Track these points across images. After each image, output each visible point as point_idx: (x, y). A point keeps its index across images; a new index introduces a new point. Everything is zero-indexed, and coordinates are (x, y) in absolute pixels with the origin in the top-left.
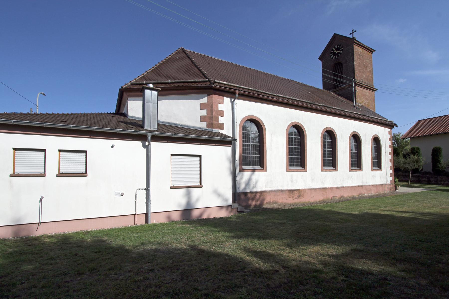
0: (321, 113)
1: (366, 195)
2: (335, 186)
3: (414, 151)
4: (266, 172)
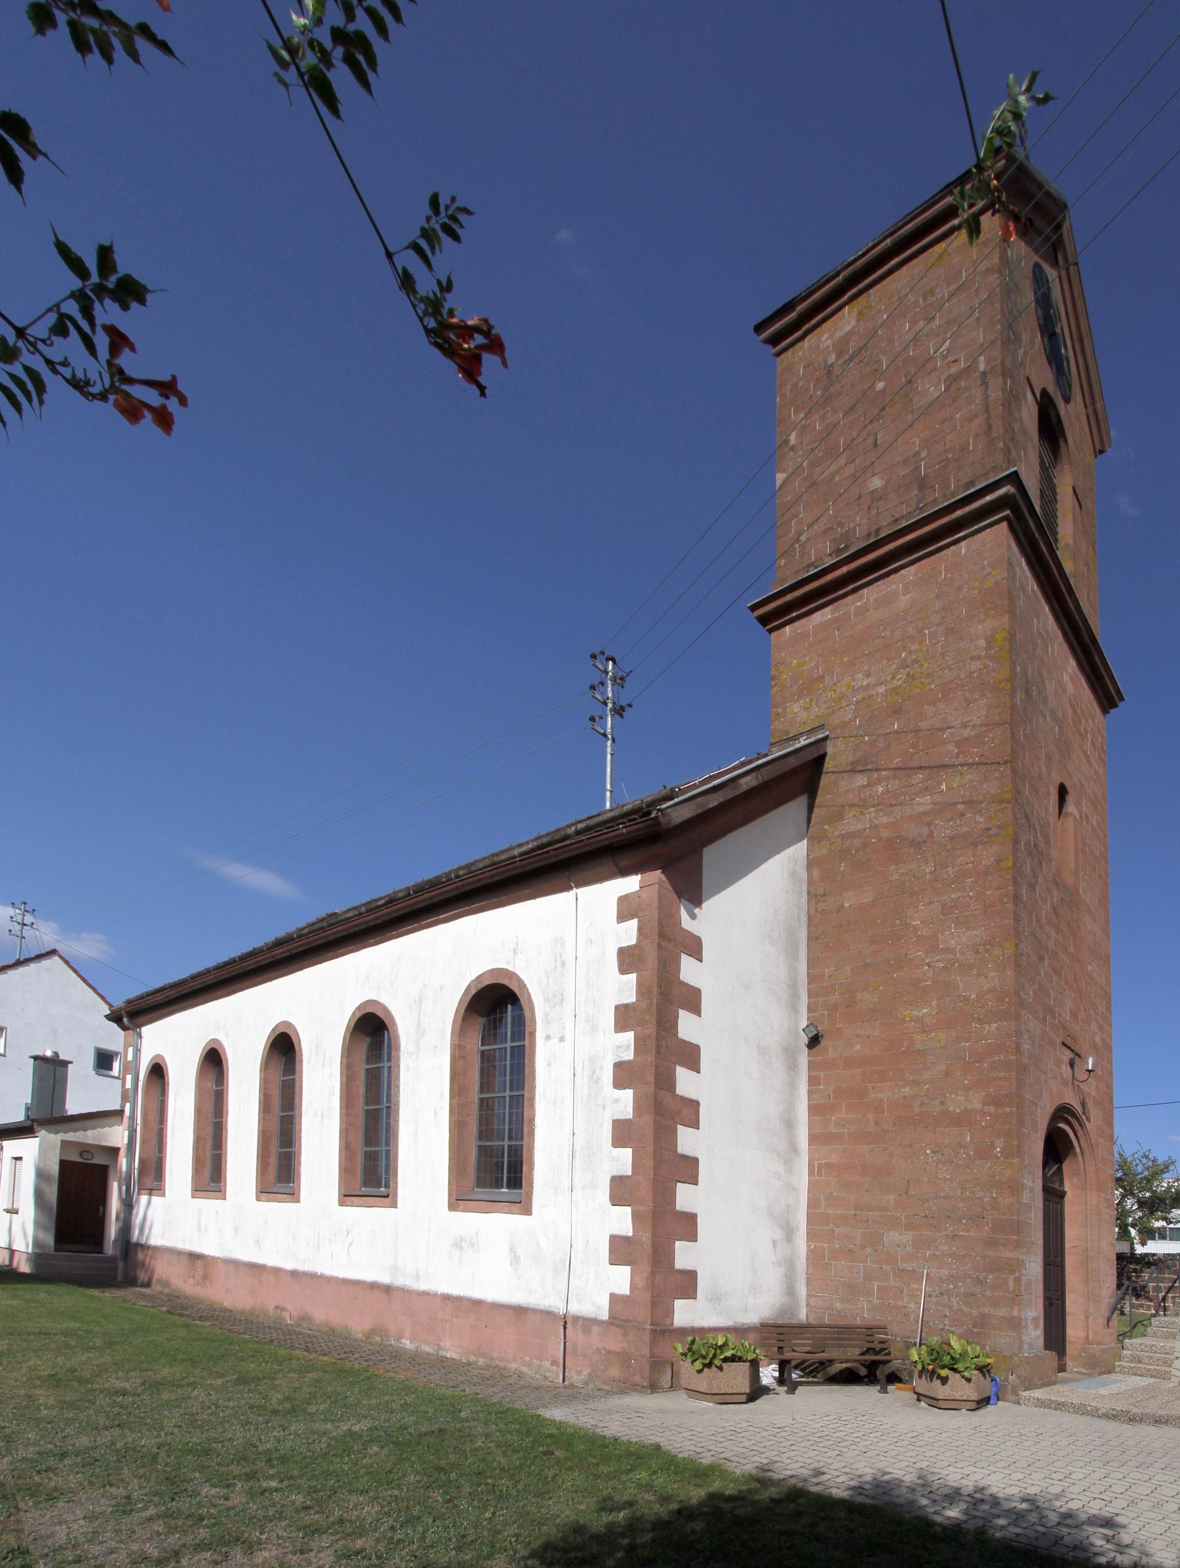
0: (276, 973)
1: (407, 1344)
2: (289, 1266)
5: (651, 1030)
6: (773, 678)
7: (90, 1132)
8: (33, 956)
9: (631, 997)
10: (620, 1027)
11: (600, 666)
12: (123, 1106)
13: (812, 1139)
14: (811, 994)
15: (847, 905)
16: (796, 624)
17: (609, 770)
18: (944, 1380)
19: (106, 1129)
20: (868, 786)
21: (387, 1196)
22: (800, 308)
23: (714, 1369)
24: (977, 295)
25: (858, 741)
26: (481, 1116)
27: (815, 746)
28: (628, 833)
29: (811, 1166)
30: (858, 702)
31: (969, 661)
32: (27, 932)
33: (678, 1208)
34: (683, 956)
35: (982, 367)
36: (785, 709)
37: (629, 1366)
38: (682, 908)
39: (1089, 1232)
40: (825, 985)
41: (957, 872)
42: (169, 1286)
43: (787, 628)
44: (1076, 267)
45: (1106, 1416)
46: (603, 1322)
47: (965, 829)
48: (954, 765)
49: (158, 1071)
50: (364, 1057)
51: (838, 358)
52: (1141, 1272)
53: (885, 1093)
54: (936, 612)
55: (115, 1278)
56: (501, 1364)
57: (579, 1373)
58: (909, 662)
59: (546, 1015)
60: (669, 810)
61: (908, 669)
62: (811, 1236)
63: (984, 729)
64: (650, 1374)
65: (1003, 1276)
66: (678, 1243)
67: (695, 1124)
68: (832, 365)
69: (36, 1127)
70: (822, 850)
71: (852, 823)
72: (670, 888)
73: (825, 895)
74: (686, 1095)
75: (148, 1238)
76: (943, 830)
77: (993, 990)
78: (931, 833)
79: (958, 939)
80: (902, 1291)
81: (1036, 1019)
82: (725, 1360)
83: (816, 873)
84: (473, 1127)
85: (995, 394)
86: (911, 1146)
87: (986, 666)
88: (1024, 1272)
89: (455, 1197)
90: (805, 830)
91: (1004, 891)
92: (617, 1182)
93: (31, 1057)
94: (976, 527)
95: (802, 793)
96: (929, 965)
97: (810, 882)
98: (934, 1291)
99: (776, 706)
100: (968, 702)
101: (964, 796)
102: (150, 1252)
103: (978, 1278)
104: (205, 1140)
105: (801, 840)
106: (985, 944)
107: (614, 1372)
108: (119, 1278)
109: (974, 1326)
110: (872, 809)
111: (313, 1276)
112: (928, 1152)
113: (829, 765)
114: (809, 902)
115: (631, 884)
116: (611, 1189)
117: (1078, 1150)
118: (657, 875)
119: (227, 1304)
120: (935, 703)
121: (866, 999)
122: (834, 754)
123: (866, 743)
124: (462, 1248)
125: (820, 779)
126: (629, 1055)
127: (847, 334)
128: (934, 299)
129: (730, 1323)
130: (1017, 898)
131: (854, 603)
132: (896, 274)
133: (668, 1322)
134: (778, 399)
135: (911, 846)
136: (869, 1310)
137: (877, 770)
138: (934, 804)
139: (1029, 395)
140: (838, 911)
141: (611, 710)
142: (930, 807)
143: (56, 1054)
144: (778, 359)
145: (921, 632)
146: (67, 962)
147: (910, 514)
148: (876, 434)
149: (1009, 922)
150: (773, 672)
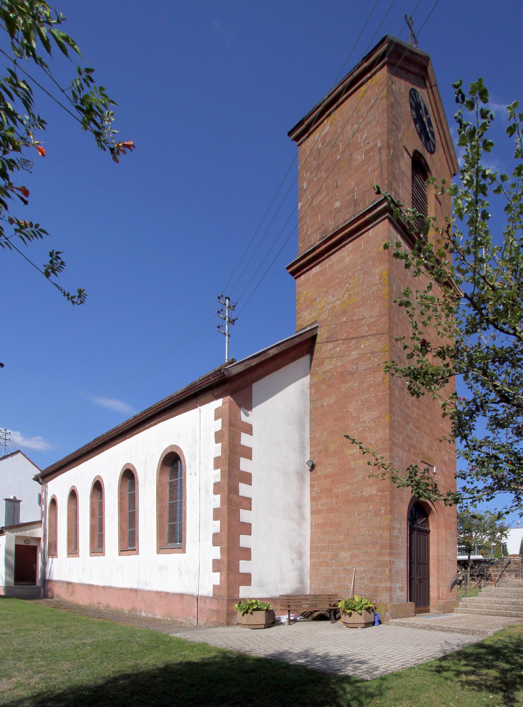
1: (143, 614)
2: (102, 584)
3: (510, 689)
4: (250, 549)
5: (226, 467)
6: (297, 301)
7: (28, 531)
8: (10, 454)
9: (219, 454)
10: (216, 467)
11: (222, 302)
12: (42, 519)
13: (312, 512)
14: (311, 446)
15: (325, 404)
16: (306, 274)
17: (227, 350)
18: (350, 615)
19: (35, 529)
20: (333, 348)
21: (135, 550)
22: (306, 123)
23: (249, 614)
24: (377, 110)
25: (330, 328)
26: (170, 511)
27: (310, 332)
28: (214, 380)
29: (311, 525)
30: (329, 309)
31: (372, 286)
32: (8, 443)
33: (241, 546)
34: (242, 433)
35: (379, 145)
36: (301, 315)
37: (219, 615)
38: (242, 412)
39: (440, 548)
40: (316, 442)
41: (367, 385)
42: (60, 598)
43: (302, 277)
44: (436, 87)
45: (421, 628)
46: (211, 597)
47: (371, 365)
48: (366, 336)
49: (54, 502)
50: (128, 488)
51: (322, 145)
52: (489, 568)
53: (339, 489)
54: (360, 264)
55: (40, 596)
56: (176, 619)
57: (202, 620)
58: (349, 289)
59: (190, 464)
60: (230, 369)
61: (349, 292)
62: (312, 557)
63: (378, 318)
64: (227, 618)
65: (384, 569)
66: (240, 561)
67: (250, 509)
68: (320, 149)
69: (4, 531)
70: (316, 379)
71: (327, 366)
72: (236, 404)
73: (316, 400)
74: (244, 495)
75: (52, 577)
76: (362, 366)
77: (381, 439)
78: (357, 368)
79: (368, 416)
80: (346, 579)
81: (403, 450)
82: (254, 610)
83: (313, 390)
84: (167, 517)
85: (384, 158)
86: (349, 513)
87: (379, 288)
88: (394, 566)
89: (159, 548)
90: (309, 370)
91: (385, 393)
92: (215, 535)
93: (4, 500)
94: (375, 223)
95: (307, 354)
96: (356, 429)
97: (311, 395)
98: (358, 577)
99: (298, 314)
100: (372, 305)
101: (370, 350)
102: (53, 583)
103: (375, 570)
104: (72, 531)
105: (306, 375)
106: (378, 418)
107: (214, 619)
108: (41, 596)
109: (373, 592)
110: (335, 359)
111: (110, 588)
112: (356, 515)
113: (318, 339)
114: (310, 404)
115: (218, 403)
116: (213, 539)
117: (434, 510)
118: (229, 398)
119: (80, 603)
120: (359, 307)
121: (333, 447)
122: (320, 334)
123: (333, 328)
124: (162, 570)
125: (315, 346)
126: (219, 480)
127: (326, 133)
128: (360, 113)
129: (269, 596)
130: (391, 396)
131: (328, 262)
132: (345, 102)
133: (236, 596)
134: (299, 167)
135: (349, 375)
136: (334, 588)
137: (337, 340)
138: (359, 354)
139: (406, 155)
140: (322, 407)
141: (228, 322)
142: (356, 356)
143: (15, 497)
144: (299, 148)
145: (354, 274)
146: (25, 456)
147: (350, 218)
148: (337, 181)
149: (387, 407)
150: (297, 298)
